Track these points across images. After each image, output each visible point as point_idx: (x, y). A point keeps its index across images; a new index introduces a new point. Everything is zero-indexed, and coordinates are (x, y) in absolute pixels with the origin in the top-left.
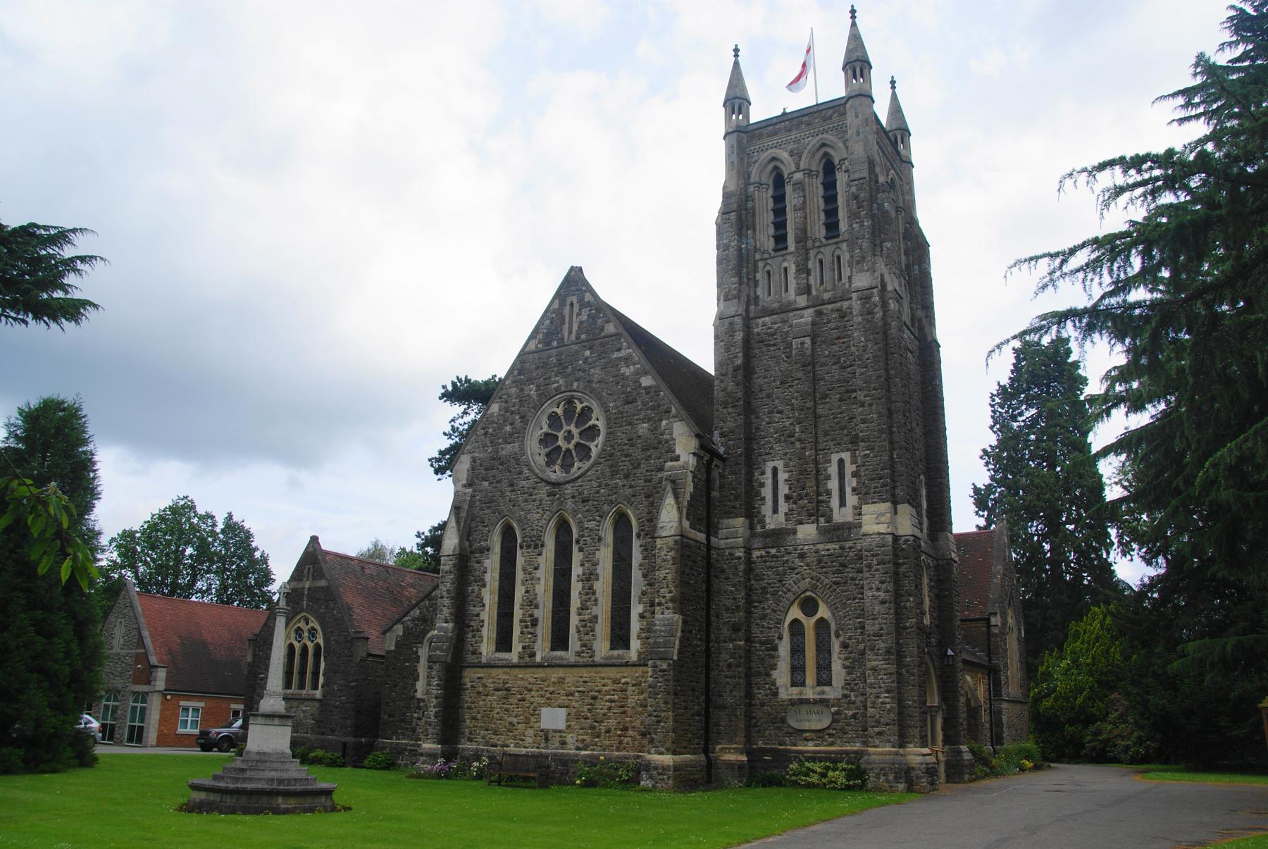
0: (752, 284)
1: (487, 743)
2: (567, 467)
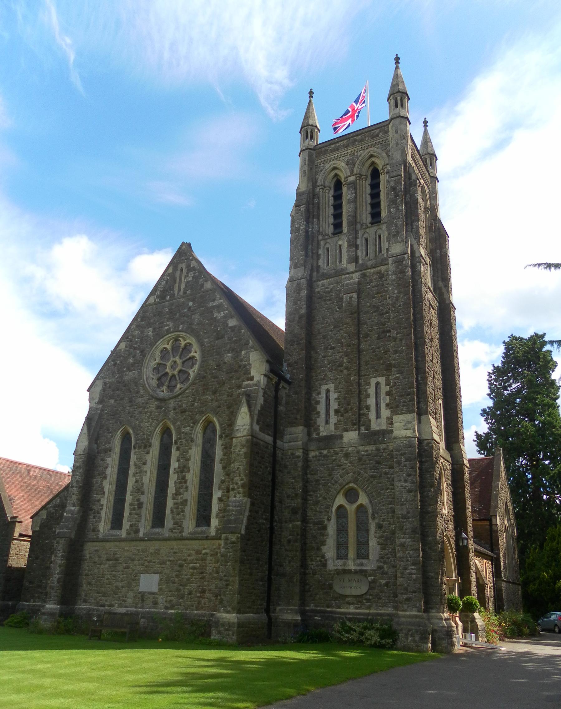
0: (315, 257)
1: (97, 604)
2: (171, 388)
